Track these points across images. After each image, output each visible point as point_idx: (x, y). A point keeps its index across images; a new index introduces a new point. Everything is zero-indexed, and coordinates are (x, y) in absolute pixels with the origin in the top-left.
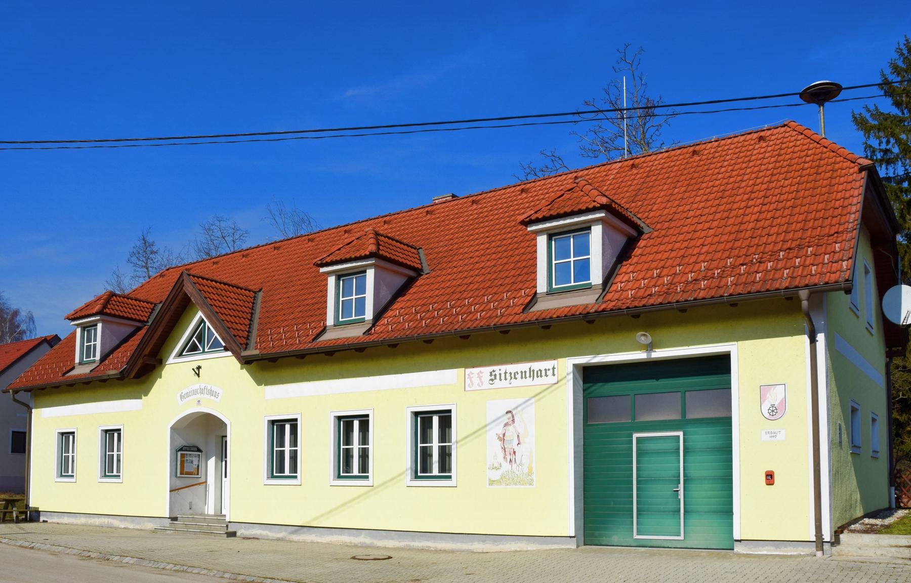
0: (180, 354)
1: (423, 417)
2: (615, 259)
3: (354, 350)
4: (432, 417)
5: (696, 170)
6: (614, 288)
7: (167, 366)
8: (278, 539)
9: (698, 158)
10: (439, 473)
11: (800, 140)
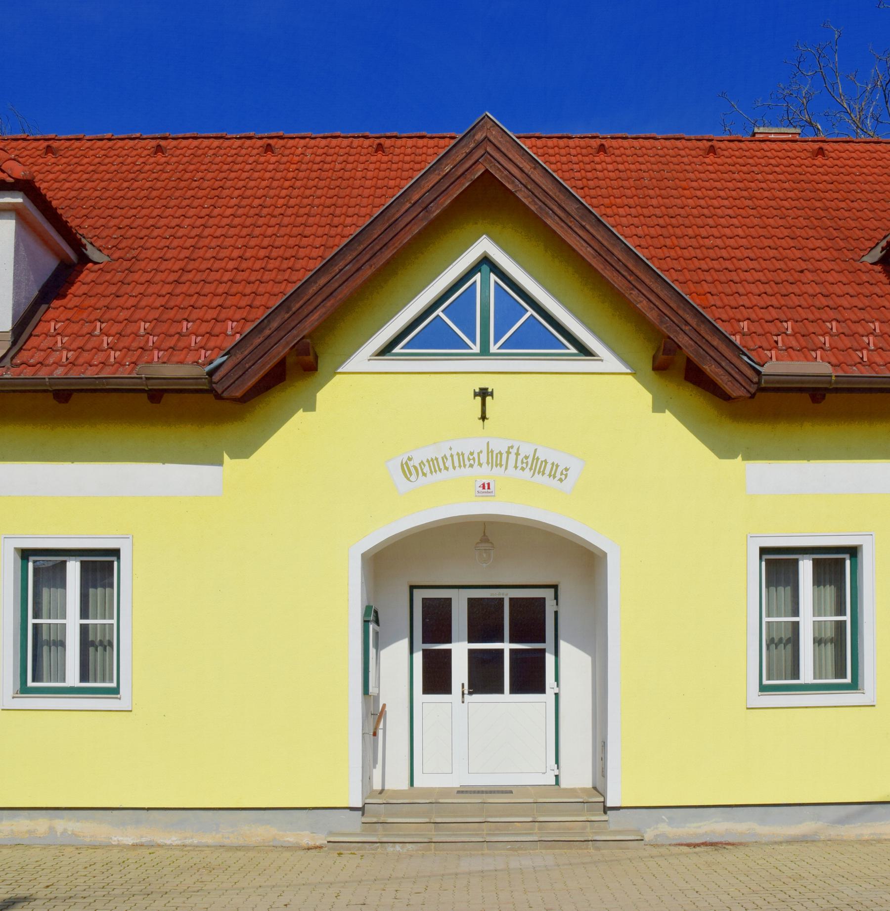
0: (386, 350)
1: (817, 559)
2: (36, 293)
3: (145, 396)
4: (796, 562)
5: (91, 177)
6: (33, 342)
7: (338, 377)
8: (791, 841)
9: (53, 160)
10: (815, 678)
11: (237, 172)
